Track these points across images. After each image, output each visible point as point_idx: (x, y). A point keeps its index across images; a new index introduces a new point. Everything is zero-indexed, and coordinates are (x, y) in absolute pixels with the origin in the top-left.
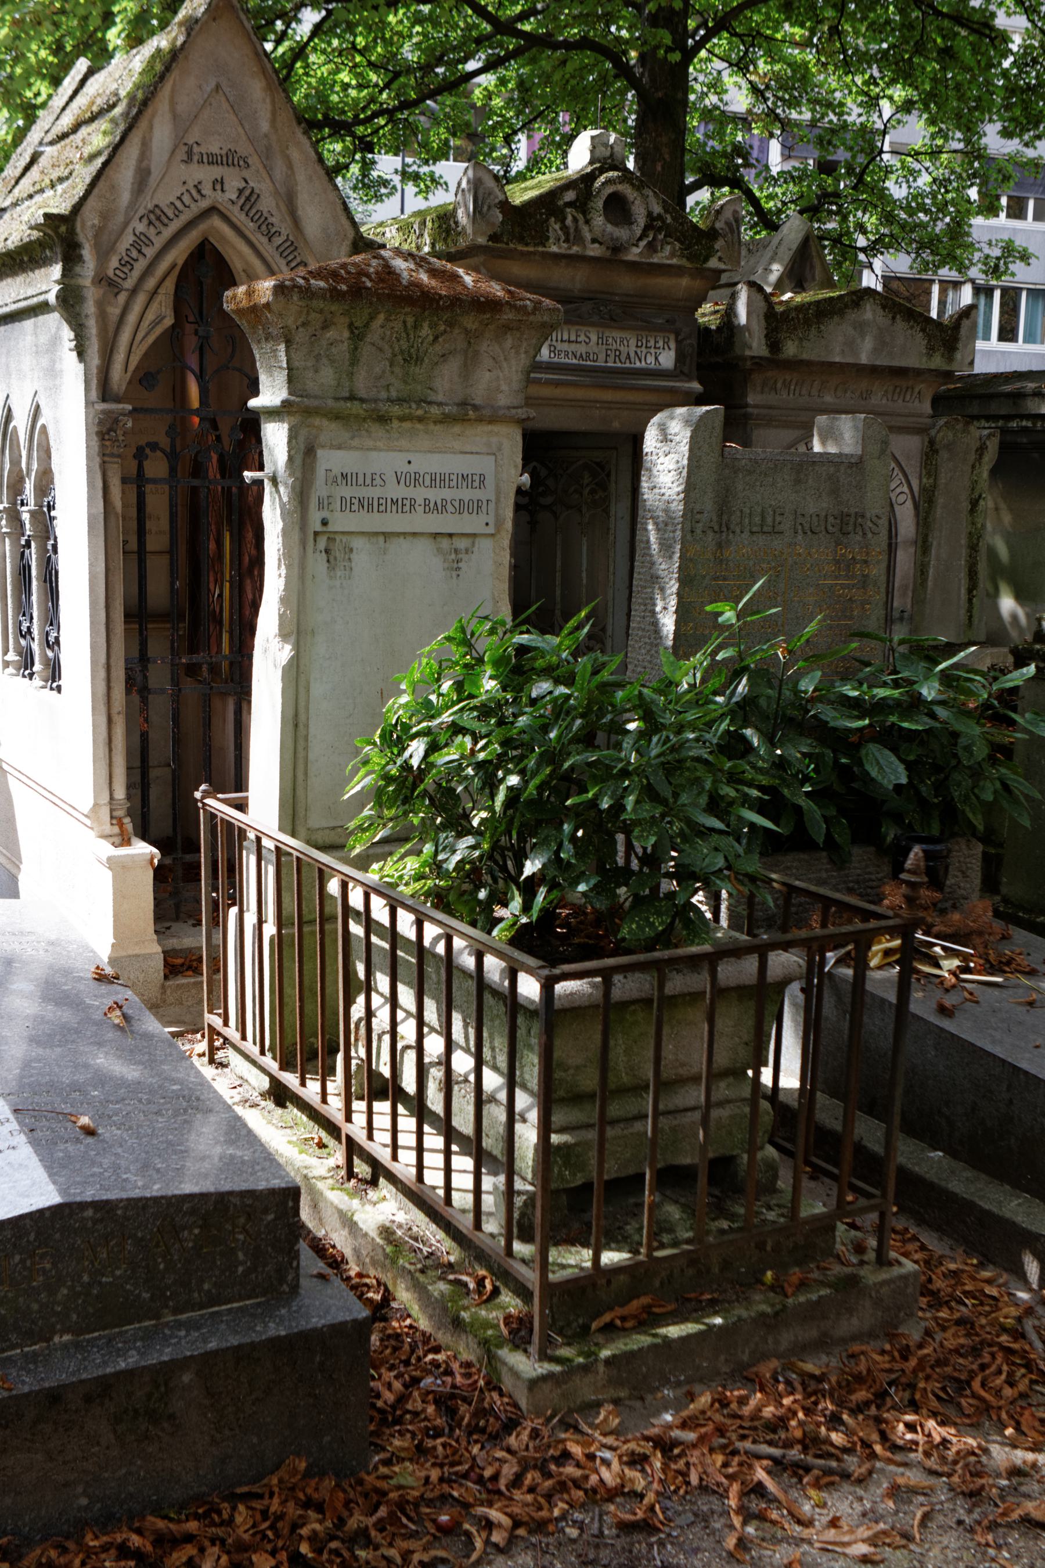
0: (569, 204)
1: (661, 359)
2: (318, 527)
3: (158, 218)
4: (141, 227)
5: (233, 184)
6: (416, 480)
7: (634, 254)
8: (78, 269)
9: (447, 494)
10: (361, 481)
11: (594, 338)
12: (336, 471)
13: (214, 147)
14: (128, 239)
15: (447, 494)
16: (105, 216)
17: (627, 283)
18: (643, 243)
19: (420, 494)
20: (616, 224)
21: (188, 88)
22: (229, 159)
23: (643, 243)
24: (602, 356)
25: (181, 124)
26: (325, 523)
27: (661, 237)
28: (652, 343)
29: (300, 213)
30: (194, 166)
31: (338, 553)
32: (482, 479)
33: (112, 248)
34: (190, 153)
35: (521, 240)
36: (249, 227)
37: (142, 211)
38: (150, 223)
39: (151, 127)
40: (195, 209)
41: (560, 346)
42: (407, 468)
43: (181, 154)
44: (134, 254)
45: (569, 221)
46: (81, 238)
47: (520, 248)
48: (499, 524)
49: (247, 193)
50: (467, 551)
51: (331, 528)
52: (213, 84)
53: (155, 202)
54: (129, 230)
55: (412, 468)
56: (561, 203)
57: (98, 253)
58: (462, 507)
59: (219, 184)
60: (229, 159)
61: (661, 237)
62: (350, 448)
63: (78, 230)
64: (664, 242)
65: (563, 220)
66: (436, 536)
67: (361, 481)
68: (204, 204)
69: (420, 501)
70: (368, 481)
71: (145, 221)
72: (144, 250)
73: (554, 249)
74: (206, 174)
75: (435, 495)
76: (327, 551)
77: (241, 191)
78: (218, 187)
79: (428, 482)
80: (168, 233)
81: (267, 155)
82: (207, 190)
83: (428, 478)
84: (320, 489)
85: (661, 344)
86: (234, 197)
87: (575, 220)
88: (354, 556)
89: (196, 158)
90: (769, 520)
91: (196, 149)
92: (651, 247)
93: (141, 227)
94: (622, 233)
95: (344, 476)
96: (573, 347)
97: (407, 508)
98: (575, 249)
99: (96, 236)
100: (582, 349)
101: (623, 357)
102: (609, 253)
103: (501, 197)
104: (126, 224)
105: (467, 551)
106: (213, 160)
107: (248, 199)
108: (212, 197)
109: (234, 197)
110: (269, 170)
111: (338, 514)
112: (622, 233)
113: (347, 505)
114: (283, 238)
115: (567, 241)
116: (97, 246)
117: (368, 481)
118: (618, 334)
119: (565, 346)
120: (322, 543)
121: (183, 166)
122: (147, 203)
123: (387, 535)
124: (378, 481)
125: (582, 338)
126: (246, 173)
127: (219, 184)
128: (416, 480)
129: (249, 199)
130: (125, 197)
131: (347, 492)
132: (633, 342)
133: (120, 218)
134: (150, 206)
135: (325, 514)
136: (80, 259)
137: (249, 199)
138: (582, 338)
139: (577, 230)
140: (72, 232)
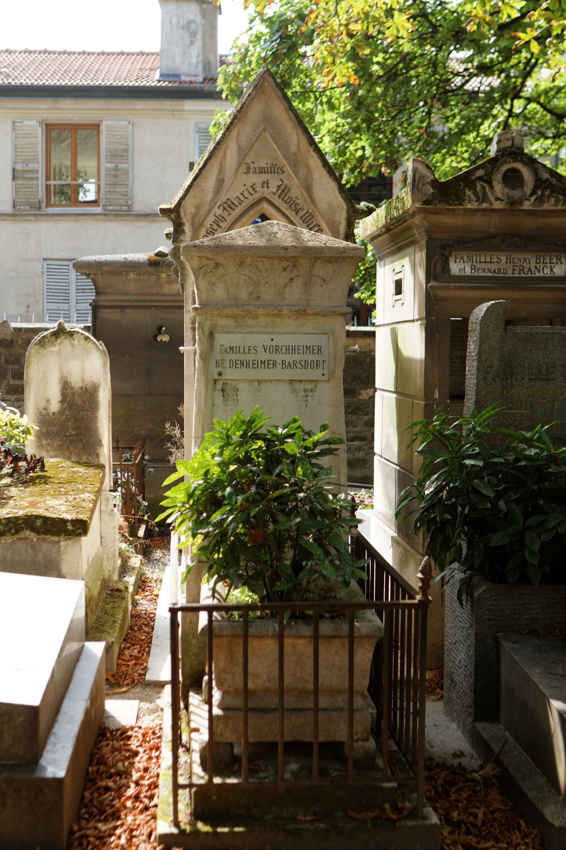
0: (480, 179)
1: (554, 270)
2: (216, 377)
3: (229, 206)
4: (219, 212)
5: (274, 182)
6: (277, 350)
7: (527, 205)
8: (182, 237)
9: (297, 357)
10: (242, 351)
11: (504, 259)
12: (227, 345)
13: (262, 164)
14: (210, 220)
15: (297, 357)
16: (198, 208)
17: (528, 223)
18: (532, 199)
19: (279, 358)
20: (514, 189)
21: (245, 131)
22: (273, 169)
23: (532, 199)
24: (510, 271)
25: (243, 153)
26: (220, 374)
27: (547, 192)
28: (548, 260)
29: (315, 196)
30: (251, 175)
31: (229, 391)
32: (320, 349)
33: (201, 224)
34: (248, 169)
35: (447, 203)
36: (284, 207)
37: (219, 203)
38: (225, 209)
39: (225, 156)
40: (251, 199)
41: (478, 265)
42: (271, 343)
43: (243, 168)
44: (215, 227)
45: (478, 189)
46: (184, 220)
47: (447, 207)
48: (332, 374)
49: (283, 187)
50: (312, 391)
51: (223, 377)
52: (262, 128)
53: (228, 197)
54: (212, 213)
55: (274, 343)
56: (474, 177)
57: (193, 228)
58: (306, 365)
59: (266, 184)
60: (273, 169)
61: (547, 192)
62: (235, 333)
63: (182, 215)
64: (549, 197)
65: (475, 189)
66: (291, 381)
67: (242, 351)
68: (257, 196)
69: (279, 361)
70: (246, 351)
71: (221, 208)
72: (221, 224)
73: (469, 206)
74: (257, 179)
75: (288, 358)
76: (223, 390)
77: (279, 187)
78: (265, 185)
79: (284, 351)
80: (235, 213)
81: (294, 165)
82: (258, 188)
83: (284, 348)
84: (217, 355)
85: (555, 260)
86: (275, 190)
87: (483, 188)
88: (239, 393)
89: (252, 170)
90: (544, 371)
91: (252, 166)
92: (540, 200)
93: (219, 212)
94: (516, 194)
95: (231, 348)
96: (489, 266)
97: (271, 366)
98: (485, 205)
99: (193, 219)
100: (495, 267)
101: (526, 271)
102: (508, 207)
103: (432, 177)
104: (210, 210)
105: (312, 391)
106: (262, 171)
107: (283, 191)
108: (261, 192)
109: (275, 190)
110: (296, 173)
111: (228, 370)
112: (516, 194)
113: (233, 364)
114: (305, 211)
115: (478, 200)
116: (193, 224)
117: (246, 351)
118: (521, 256)
119: (483, 266)
120: (219, 386)
121: (244, 176)
122: (223, 198)
123: (259, 382)
124: (253, 351)
125: (495, 259)
126: (282, 176)
127: (266, 184)
128: (277, 350)
129: (283, 191)
130: (210, 195)
131: (233, 357)
132: (533, 260)
133: (206, 208)
134: (225, 200)
135: (220, 369)
136: (183, 232)
137: (283, 191)
138: (495, 259)
139: (485, 193)
140: (178, 216)
